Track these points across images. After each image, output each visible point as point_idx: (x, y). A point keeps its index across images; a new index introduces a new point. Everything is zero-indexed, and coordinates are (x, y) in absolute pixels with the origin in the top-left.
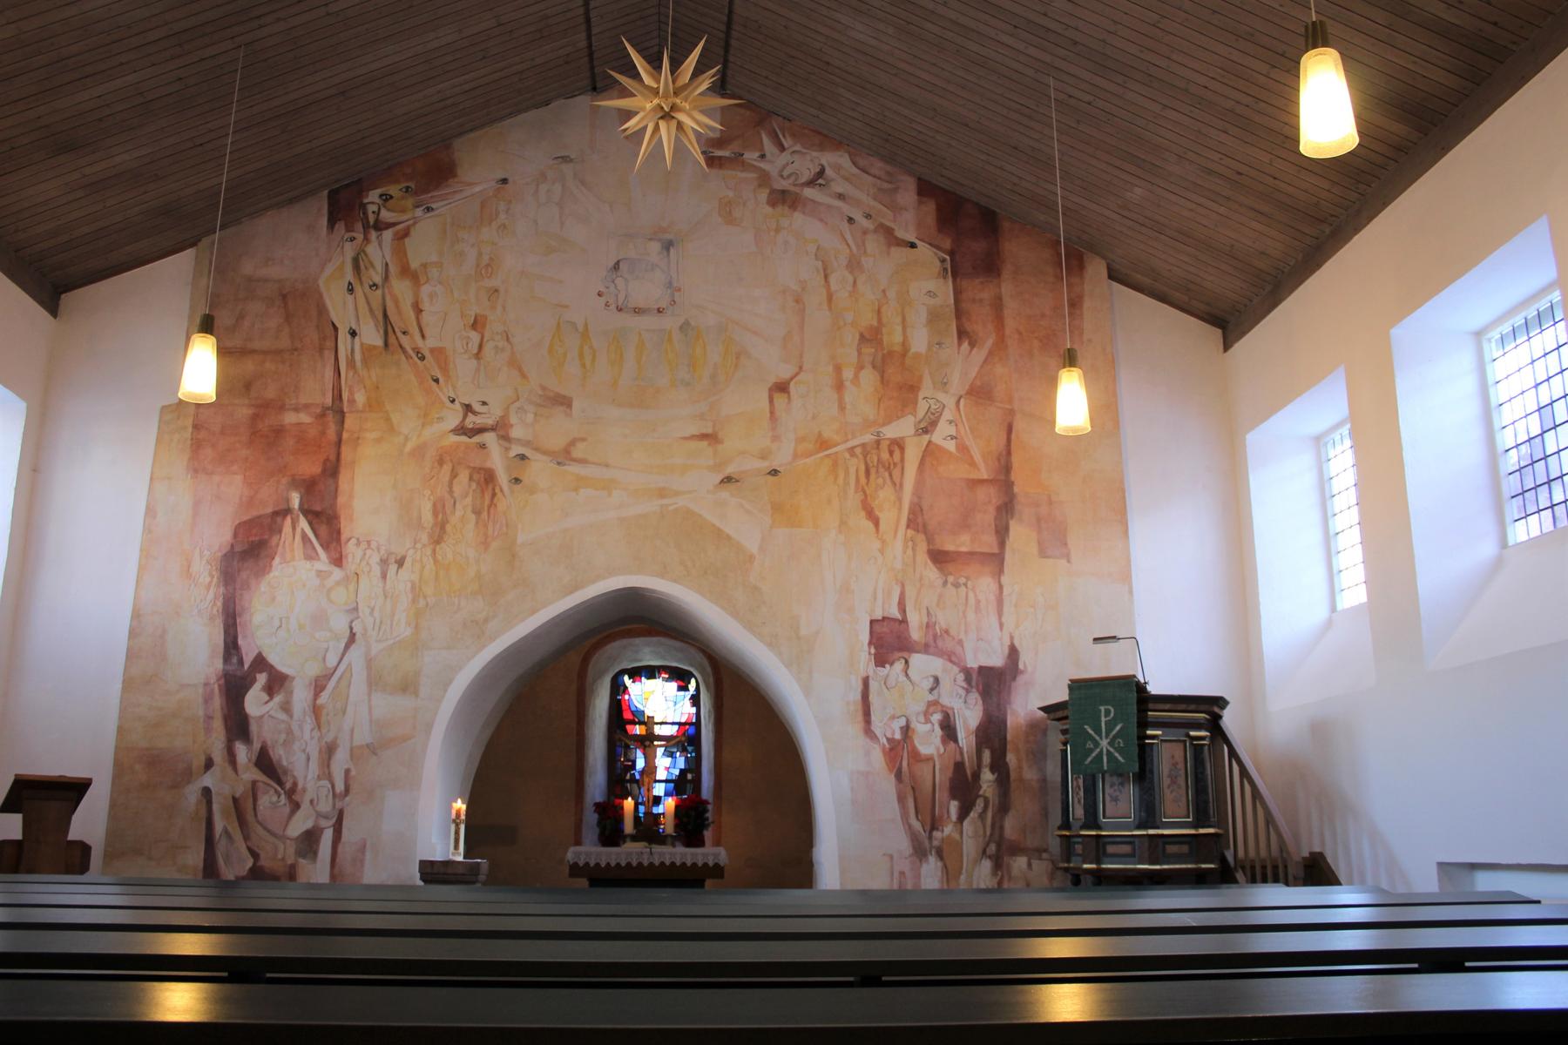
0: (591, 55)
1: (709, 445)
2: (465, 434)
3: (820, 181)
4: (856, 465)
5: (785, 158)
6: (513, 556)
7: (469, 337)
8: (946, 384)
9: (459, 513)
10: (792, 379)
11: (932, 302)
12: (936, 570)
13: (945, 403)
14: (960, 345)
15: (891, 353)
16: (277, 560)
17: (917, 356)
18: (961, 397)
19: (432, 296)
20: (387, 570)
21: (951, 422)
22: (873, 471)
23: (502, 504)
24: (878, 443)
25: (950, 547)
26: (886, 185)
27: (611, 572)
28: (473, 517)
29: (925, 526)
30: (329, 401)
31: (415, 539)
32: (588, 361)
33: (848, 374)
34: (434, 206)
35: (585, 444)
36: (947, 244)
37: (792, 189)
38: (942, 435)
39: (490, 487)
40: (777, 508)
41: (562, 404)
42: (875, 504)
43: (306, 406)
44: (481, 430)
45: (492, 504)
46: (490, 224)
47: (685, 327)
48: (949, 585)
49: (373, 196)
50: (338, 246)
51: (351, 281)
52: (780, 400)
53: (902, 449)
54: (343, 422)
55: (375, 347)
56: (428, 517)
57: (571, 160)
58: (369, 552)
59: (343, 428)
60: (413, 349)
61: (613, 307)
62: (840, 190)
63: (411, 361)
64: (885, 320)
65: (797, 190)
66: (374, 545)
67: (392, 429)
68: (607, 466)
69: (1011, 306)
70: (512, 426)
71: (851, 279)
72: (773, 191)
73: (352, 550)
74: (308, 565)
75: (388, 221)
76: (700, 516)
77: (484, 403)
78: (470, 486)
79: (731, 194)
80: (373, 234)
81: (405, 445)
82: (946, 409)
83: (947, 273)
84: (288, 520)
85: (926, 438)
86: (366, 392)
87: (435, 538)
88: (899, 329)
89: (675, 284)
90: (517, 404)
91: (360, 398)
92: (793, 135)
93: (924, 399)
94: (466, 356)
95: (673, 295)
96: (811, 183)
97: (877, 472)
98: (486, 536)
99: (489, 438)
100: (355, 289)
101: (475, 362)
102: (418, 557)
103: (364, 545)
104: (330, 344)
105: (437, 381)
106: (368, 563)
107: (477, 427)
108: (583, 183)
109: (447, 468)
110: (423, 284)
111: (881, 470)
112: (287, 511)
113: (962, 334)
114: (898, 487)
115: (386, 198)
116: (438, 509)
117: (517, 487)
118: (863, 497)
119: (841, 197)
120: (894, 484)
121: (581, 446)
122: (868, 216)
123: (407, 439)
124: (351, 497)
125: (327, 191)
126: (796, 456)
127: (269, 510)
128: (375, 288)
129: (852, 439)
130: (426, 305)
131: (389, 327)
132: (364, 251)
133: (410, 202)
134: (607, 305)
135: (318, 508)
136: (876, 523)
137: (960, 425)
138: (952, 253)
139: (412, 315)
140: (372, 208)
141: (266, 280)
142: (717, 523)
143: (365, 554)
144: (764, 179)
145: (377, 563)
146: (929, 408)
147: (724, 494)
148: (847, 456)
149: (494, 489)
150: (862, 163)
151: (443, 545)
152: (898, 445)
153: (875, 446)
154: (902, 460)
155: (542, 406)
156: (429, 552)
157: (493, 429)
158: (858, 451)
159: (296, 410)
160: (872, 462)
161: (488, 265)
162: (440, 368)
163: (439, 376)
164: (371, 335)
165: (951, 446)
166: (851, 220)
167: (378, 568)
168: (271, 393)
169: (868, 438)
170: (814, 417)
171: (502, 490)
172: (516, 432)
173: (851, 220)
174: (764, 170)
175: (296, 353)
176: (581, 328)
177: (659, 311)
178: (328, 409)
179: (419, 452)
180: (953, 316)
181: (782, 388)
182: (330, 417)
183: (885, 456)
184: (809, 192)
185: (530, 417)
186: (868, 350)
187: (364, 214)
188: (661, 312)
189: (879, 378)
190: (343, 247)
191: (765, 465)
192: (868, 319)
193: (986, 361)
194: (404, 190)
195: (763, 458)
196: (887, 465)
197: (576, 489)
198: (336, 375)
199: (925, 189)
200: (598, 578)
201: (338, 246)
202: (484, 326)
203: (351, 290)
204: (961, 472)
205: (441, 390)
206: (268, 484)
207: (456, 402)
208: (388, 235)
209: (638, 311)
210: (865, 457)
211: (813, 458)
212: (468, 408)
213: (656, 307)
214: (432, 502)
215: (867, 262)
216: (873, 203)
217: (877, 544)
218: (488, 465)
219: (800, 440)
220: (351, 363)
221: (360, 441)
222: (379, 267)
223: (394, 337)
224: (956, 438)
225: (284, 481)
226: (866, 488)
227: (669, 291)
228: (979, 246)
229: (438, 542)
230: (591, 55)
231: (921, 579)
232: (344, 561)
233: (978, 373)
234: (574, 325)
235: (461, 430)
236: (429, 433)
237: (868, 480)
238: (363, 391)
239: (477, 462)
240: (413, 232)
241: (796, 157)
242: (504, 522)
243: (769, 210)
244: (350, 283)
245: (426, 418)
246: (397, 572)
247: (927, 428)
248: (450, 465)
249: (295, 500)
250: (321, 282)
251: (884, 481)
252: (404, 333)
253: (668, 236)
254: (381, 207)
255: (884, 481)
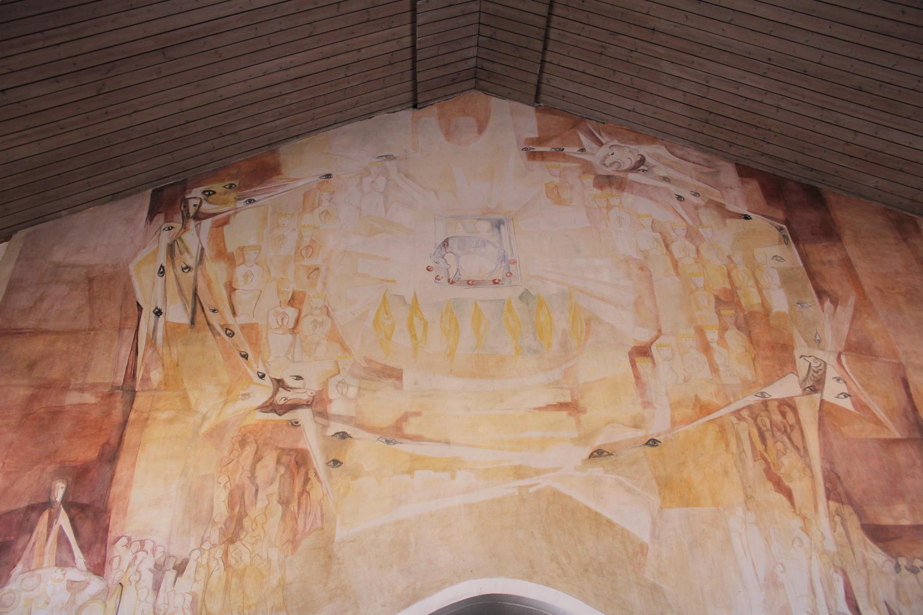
0: (414, 59)
1: (570, 414)
2: (275, 412)
3: (642, 167)
4: (745, 429)
5: (602, 152)
6: (330, 557)
7: (284, 313)
8: (819, 341)
9: (261, 504)
10: (652, 343)
11: (781, 265)
12: (880, 551)
13: (826, 361)
14: (822, 303)
15: (752, 314)
16: (20, 567)
17: (780, 315)
18: (840, 354)
19: (246, 276)
20: (162, 579)
21: (838, 380)
22: (768, 435)
23: (316, 492)
24: (765, 404)
25: (887, 521)
26: (706, 170)
27: (459, 576)
28: (279, 508)
29: (848, 496)
30: (120, 380)
31: (203, 537)
32: (419, 334)
33: (712, 336)
34: (255, 198)
35: (419, 418)
36: (780, 215)
37: (617, 174)
38: (832, 391)
39: (303, 471)
40: (665, 485)
41: (390, 376)
42: (781, 473)
43: (94, 386)
44: (294, 407)
45: (304, 491)
46: (313, 210)
47: (525, 296)
48: (904, 571)
49: (197, 192)
50: (155, 234)
51: (164, 265)
52: (643, 364)
53: (794, 409)
54: (132, 401)
55: (180, 325)
56: (221, 509)
57: (395, 158)
58: (141, 555)
59: (131, 408)
60: (222, 326)
61: (444, 280)
62: (663, 173)
63: (218, 338)
64: (737, 284)
65: (622, 175)
66: (149, 546)
67: (187, 407)
68: (448, 442)
69: (862, 267)
70: (330, 401)
71: (693, 248)
72: (598, 177)
73: (120, 554)
74: (58, 573)
75: (207, 212)
76: (570, 497)
77: (299, 378)
78: (277, 470)
79: (557, 180)
80: (192, 224)
81: (201, 425)
82: (828, 366)
83: (788, 240)
84: (46, 516)
85: (817, 396)
86: (164, 369)
87: (230, 536)
88: (754, 290)
89: (509, 258)
90: (339, 378)
91: (156, 376)
92: (610, 134)
93: (801, 357)
94: (280, 332)
95: (509, 268)
96: (634, 169)
97: (773, 436)
98: (295, 532)
99: (303, 415)
100: (167, 272)
101: (291, 336)
102: (204, 562)
103: (136, 546)
104: (132, 323)
105: (245, 356)
106: (137, 570)
107: (289, 403)
108: (407, 176)
109: (250, 450)
110: (239, 265)
111: (778, 434)
112: (47, 504)
113: (821, 294)
114: (803, 451)
115: (209, 194)
116: (236, 499)
117: (336, 471)
118: (764, 466)
119: (665, 179)
120: (797, 448)
121: (413, 421)
122: (696, 194)
123: (204, 418)
124: (129, 486)
125: (150, 191)
126: (674, 423)
127: (24, 504)
128: (187, 270)
129: (735, 401)
130: (240, 284)
131: (198, 306)
132: (180, 238)
133: (232, 196)
134: (437, 278)
135: (85, 500)
136: (789, 495)
137: (850, 383)
138: (787, 223)
139: (224, 293)
140: (192, 202)
141: (74, 266)
142: (593, 505)
143: (136, 558)
144: (587, 167)
145: (150, 570)
146: (810, 365)
147: (597, 470)
148: (735, 420)
149: (307, 474)
150: (678, 152)
151: (238, 544)
152: (787, 405)
153: (763, 408)
154: (798, 421)
155: (367, 379)
156: (219, 553)
157: (308, 405)
158: (745, 413)
159: (81, 390)
160: (765, 426)
161: (308, 246)
162: (251, 344)
163: (249, 352)
164: (178, 314)
165: (847, 404)
166: (680, 198)
167: (151, 575)
168: (56, 373)
169: (752, 399)
170: (686, 381)
171: (316, 474)
172: (336, 408)
173: (680, 198)
174: (586, 161)
175: (92, 333)
176: (409, 300)
177: (495, 282)
178: (118, 388)
179: (216, 434)
180: (806, 277)
181: (643, 351)
182: (119, 396)
183: (778, 418)
184: (632, 176)
185: (352, 391)
186: (727, 312)
187: (185, 207)
188: (497, 283)
189: (746, 338)
190: (160, 235)
191: (641, 434)
192: (720, 283)
193: (853, 317)
194: (228, 187)
195: (636, 426)
196: (783, 428)
197: (410, 472)
198: (133, 353)
199: (745, 172)
200: (442, 585)
201: (155, 234)
202: (302, 302)
203: (162, 272)
204: (867, 431)
205: (249, 365)
206: (30, 472)
207: (267, 377)
208: (207, 224)
209: (470, 283)
210: (755, 419)
211: (695, 424)
212: (280, 384)
213: (491, 278)
214: (228, 491)
215: (706, 232)
216: (696, 183)
217: (797, 523)
218: (301, 445)
219: (675, 406)
220: (151, 342)
221: (149, 422)
222: (194, 251)
223: (202, 315)
224: (850, 396)
225: (50, 468)
226: (765, 454)
227: (504, 264)
228: (812, 216)
229: (232, 541)
230: (414, 59)
231: (865, 563)
232: (107, 566)
233: (850, 329)
234: (402, 298)
235: (270, 407)
236: (230, 411)
237: (766, 445)
238: (161, 369)
239: (286, 440)
240: (232, 220)
241: (615, 150)
242: (319, 514)
243: (597, 191)
244: (162, 267)
245: (229, 395)
246: (175, 582)
247: (815, 385)
248: (254, 446)
249: (59, 491)
250: (131, 267)
251: (785, 445)
252: (214, 311)
253: (497, 217)
254: (204, 201)
255: (785, 445)
